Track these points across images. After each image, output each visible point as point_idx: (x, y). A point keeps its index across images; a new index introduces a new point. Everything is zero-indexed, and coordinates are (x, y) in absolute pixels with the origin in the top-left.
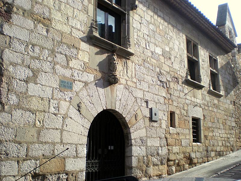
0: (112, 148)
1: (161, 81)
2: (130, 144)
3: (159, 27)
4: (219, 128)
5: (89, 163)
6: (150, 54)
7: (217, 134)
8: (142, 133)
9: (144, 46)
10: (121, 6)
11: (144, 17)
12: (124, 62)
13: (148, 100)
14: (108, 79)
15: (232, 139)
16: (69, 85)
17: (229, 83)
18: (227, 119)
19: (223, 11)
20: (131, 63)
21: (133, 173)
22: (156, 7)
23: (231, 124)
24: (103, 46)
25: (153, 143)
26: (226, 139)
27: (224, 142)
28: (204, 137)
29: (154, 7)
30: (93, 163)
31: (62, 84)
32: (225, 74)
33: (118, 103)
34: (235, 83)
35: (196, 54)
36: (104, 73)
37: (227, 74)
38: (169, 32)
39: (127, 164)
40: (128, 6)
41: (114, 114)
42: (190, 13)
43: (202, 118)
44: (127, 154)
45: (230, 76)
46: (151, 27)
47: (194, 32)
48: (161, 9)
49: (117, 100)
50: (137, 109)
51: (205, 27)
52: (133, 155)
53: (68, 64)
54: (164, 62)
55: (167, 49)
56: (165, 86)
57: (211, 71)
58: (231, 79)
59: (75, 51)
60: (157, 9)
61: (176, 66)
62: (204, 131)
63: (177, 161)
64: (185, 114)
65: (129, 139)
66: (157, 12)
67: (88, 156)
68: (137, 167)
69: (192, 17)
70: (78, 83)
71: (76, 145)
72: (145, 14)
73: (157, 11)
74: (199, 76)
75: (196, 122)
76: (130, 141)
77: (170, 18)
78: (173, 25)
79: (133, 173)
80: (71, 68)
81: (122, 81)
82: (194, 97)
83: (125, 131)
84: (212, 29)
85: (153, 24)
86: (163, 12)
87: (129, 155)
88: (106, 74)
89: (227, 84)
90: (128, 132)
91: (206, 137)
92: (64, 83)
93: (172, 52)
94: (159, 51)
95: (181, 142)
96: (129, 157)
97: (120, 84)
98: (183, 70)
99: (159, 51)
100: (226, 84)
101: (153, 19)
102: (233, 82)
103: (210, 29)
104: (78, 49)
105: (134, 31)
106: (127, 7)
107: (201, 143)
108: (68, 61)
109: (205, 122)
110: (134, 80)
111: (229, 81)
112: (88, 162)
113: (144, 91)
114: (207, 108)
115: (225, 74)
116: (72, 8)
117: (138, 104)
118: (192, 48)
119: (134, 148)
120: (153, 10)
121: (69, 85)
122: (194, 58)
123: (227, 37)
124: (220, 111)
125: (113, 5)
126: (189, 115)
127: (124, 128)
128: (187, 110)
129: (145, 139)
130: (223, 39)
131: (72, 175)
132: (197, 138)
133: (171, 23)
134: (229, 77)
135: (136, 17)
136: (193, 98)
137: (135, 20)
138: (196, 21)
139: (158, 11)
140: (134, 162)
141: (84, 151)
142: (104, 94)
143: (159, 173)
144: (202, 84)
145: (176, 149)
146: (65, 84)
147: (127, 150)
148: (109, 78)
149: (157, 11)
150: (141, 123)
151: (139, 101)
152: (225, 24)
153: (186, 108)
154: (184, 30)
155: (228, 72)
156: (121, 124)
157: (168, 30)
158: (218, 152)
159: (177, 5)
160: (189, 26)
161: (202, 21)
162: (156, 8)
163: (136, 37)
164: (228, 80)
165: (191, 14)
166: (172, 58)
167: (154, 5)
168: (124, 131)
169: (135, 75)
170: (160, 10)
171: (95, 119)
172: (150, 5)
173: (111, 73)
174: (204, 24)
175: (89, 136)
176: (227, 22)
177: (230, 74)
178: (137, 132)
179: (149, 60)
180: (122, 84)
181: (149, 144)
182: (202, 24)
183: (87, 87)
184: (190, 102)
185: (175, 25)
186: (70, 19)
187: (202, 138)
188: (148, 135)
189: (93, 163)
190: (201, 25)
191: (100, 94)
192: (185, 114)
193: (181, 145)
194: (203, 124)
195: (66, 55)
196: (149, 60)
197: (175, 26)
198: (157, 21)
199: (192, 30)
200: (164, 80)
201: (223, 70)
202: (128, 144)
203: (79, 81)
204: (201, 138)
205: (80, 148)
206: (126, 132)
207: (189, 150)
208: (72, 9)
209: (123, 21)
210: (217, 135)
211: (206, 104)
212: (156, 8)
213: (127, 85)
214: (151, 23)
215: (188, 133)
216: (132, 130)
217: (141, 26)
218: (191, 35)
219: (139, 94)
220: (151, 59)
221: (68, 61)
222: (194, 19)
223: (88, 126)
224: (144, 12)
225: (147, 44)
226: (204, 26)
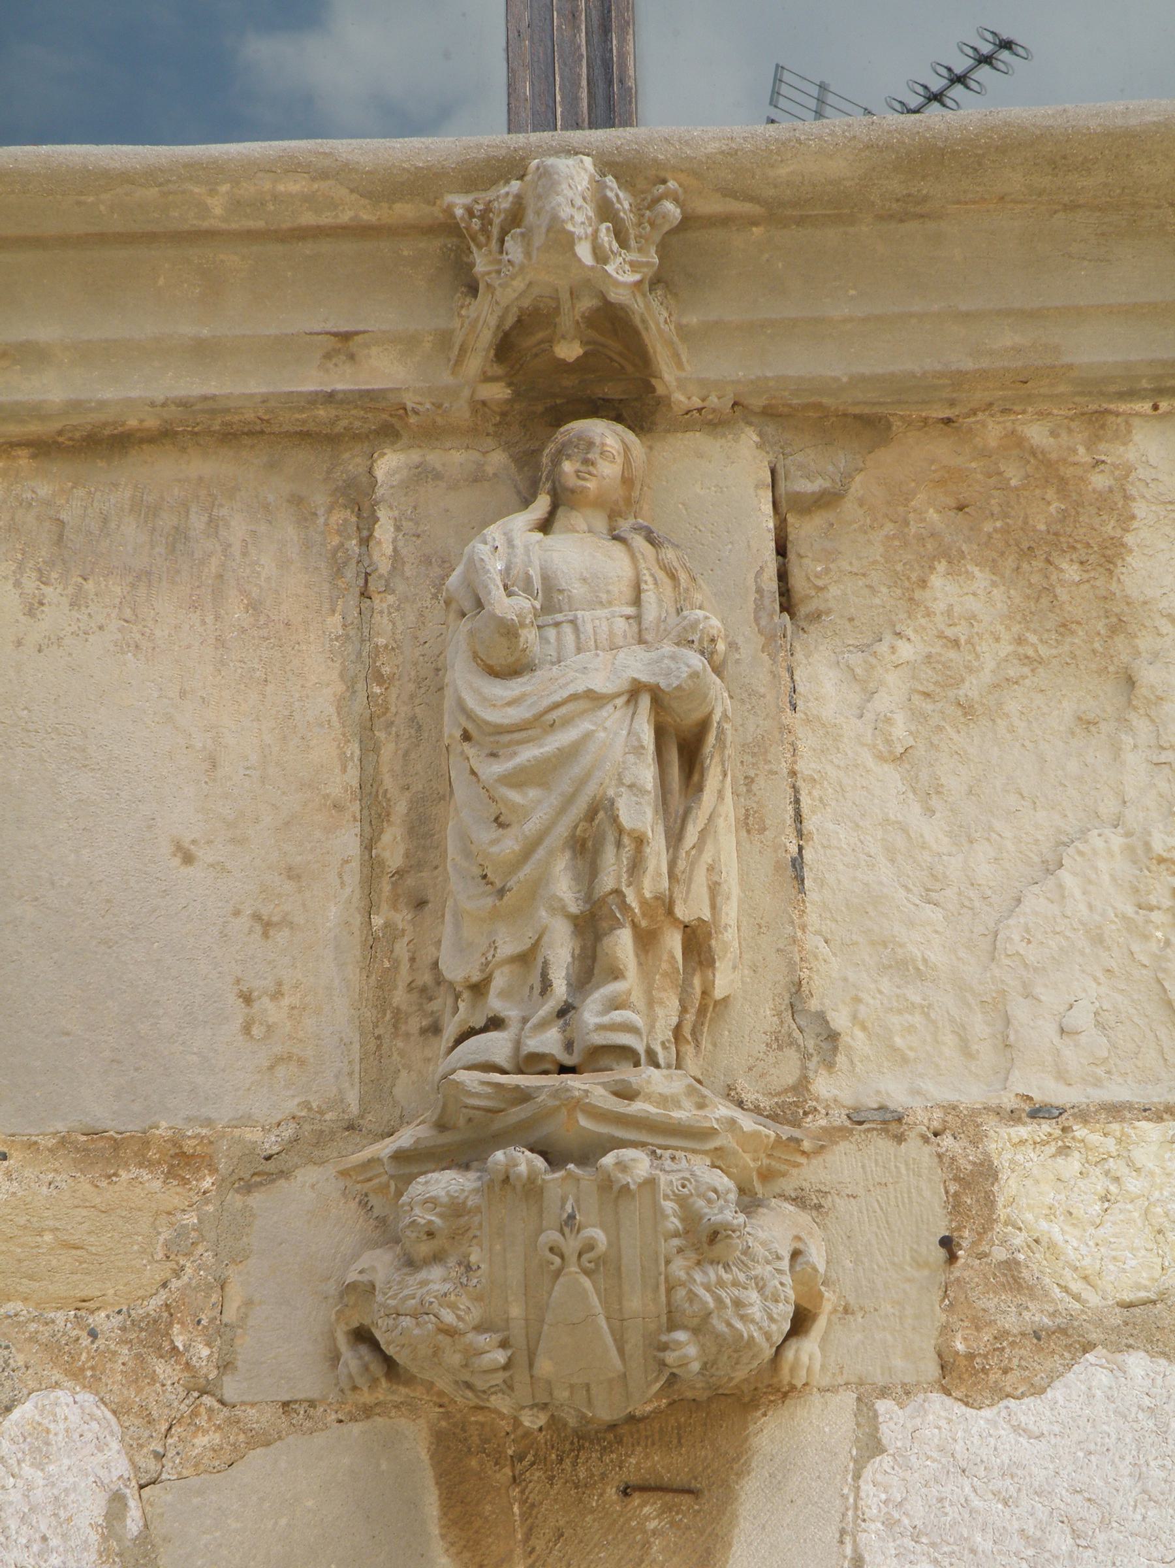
36: (181, 1161)
88: (264, 1171)
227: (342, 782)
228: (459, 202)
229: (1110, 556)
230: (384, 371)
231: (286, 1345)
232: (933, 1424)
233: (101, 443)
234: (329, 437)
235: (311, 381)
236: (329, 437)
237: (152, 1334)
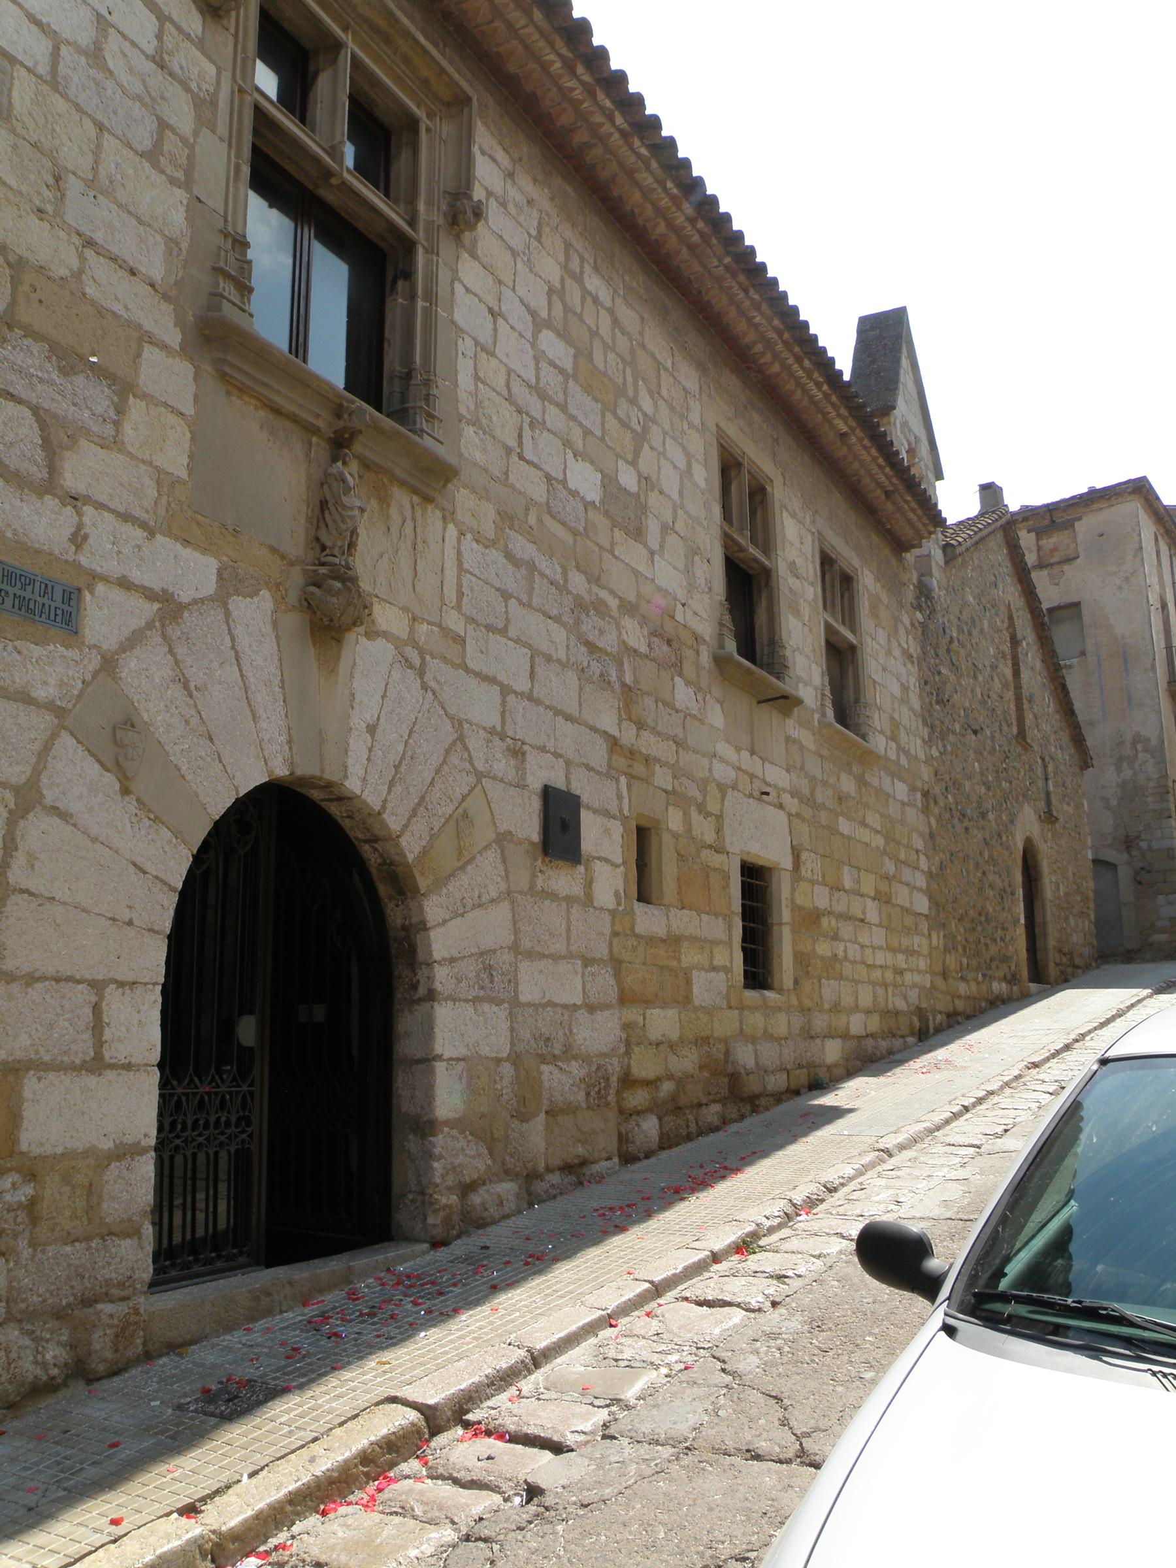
0: (319, 1013)
1: (592, 648)
2: (422, 991)
3: (590, 355)
4: (862, 921)
5: (223, 1097)
6: (538, 492)
7: (854, 952)
8: (492, 927)
9: (512, 443)
10: (387, 195)
11: (511, 284)
12: (402, 514)
13: (523, 743)
14: (327, 609)
15: (917, 978)
16: (59, 604)
17: (904, 700)
18: (894, 877)
19: (885, 336)
20: (439, 524)
21: (441, 1157)
22: (575, 243)
23: (911, 903)
24: (239, 369)
25: (547, 984)
26: (889, 976)
27: (880, 991)
28: (795, 957)
29: (568, 245)
30: (201, 1101)
31: (11, 590)
32: (889, 653)
33: (358, 745)
34: (931, 704)
35: (765, 538)
36: (283, 557)
37: (897, 652)
38: (636, 390)
39: (405, 1101)
40: (430, 203)
41: (334, 810)
42: (742, 313)
43: (787, 863)
44: (405, 1048)
45: (909, 665)
46: (550, 342)
47: (756, 417)
48: (599, 261)
49: (393, 744)
50: (465, 789)
51: (811, 398)
52: (438, 1049)
53: (53, 468)
54: (608, 546)
55: (628, 479)
56: (614, 678)
57: (828, 626)
58: (913, 680)
59: (100, 398)
60: (582, 259)
61: (667, 575)
62: (793, 931)
63: (667, 1087)
64: (710, 838)
65: (421, 957)
66: (582, 272)
67: (175, 1061)
68: (458, 1124)
69: (751, 337)
70: (117, 595)
71: (98, 986)
72: (520, 265)
73: (582, 267)
74: (774, 643)
75: (755, 880)
76: (422, 973)
77: (642, 319)
78: (659, 363)
79: (441, 1157)
80: (74, 500)
81: (386, 617)
82: (753, 753)
83: (395, 915)
84: (840, 416)
85: (558, 334)
86: (608, 281)
87: (419, 1054)
88: (292, 564)
89: (896, 704)
90: (415, 920)
91: (801, 960)
92: (23, 588)
93: (653, 499)
94: (585, 480)
95: (689, 982)
96: (419, 1061)
97: (371, 635)
98: (703, 609)
99: (585, 480)
100: (892, 703)
101: (558, 307)
102: (921, 696)
103: (834, 414)
104: (123, 388)
105: (457, 350)
106: (421, 207)
107: (780, 991)
108: (51, 450)
109: (803, 886)
110: (454, 621)
111: (905, 688)
112: (172, 1095)
113: (505, 690)
114: (807, 813)
115: (889, 653)
116: (87, 122)
117: (471, 761)
118: (743, 498)
119: (444, 1015)
120: (562, 259)
121: (59, 604)
122: (753, 551)
123: (897, 452)
124: (867, 831)
125: (346, 175)
126: (728, 841)
127: (391, 898)
128: (719, 818)
129: (504, 959)
130: (885, 474)
131: (66, 1179)
132: (758, 971)
133: (650, 347)
134: (903, 670)
135: (469, 270)
136: (745, 754)
137: (468, 290)
138: (768, 358)
139: (588, 268)
140: (448, 1097)
141: (139, 1028)
142: (277, 681)
143: (580, 1150)
144: (787, 687)
145: (663, 1022)
146: (27, 594)
147: (405, 1022)
148: (312, 589)
149: (582, 267)
150: (486, 872)
151: (476, 742)
152: (894, 408)
153: (713, 806)
154: (710, 396)
155: (900, 645)
156: (374, 871)
157: (635, 384)
158: (853, 1037)
159: (685, 253)
160: (732, 381)
161: (796, 367)
162: (577, 251)
163: (465, 380)
164: (902, 685)
165: (750, 320)
166: (653, 529)
167: (569, 234)
168: (388, 912)
169: (460, 594)
170: (596, 268)
171: (220, 828)
172: (546, 230)
173: (323, 564)
174: (804, 380)
175: (179, 940)
176: (901, 403)
177: (910, 657)
178: (458, 926)
179: (532, 519)
180: (386, 635)
181: (528, 993)
182: (798, 383)
183: (174, 632)
184: (732, 774)
185: (669, 364)
186: (73, 186)
187: (785, 968)
188: (526, 944)
189: (201, 1101)
190: (791, 385)
191: (252, 680)
192: (710, 838)
193: (688, 999)
194: (789, 896)
195: (36, 411)
196: (532, 519)
197: (666, 369)
198: (582, 320)
199: (745, 407)
200: (608, 641)
201: (880, 630)
202: (414, 987)
203: (125, 584)
204: (781, 964)
205: (117, 1006)
206: (399, 922)
207: (724, 1025)
208: (92, 131)
209: (400, 283)
210: (850, 955)
211: (806, 791)
212: (578, 253)
213: (416, 645)
214: (549, 324)
215: (725, 938)
216: (433, 909)
217: (495, 330)
218: (742, 431)
219: (482, 707)
220: (547, 519)
221: (51, 450)
222: (759, 348)
223: (177, 868)
224: (514, 254)
225: (527, 434)
226: (806, 392)
227: (305, 497)
228: (345, 404)
229: (389, 506)
230: (320, 423)
231: (293, 597)
232: (363, 640)
233: (278, 412)
234: (311, 430)
235: (311, 419)
236: (311, 430)
237: (278, 585)
